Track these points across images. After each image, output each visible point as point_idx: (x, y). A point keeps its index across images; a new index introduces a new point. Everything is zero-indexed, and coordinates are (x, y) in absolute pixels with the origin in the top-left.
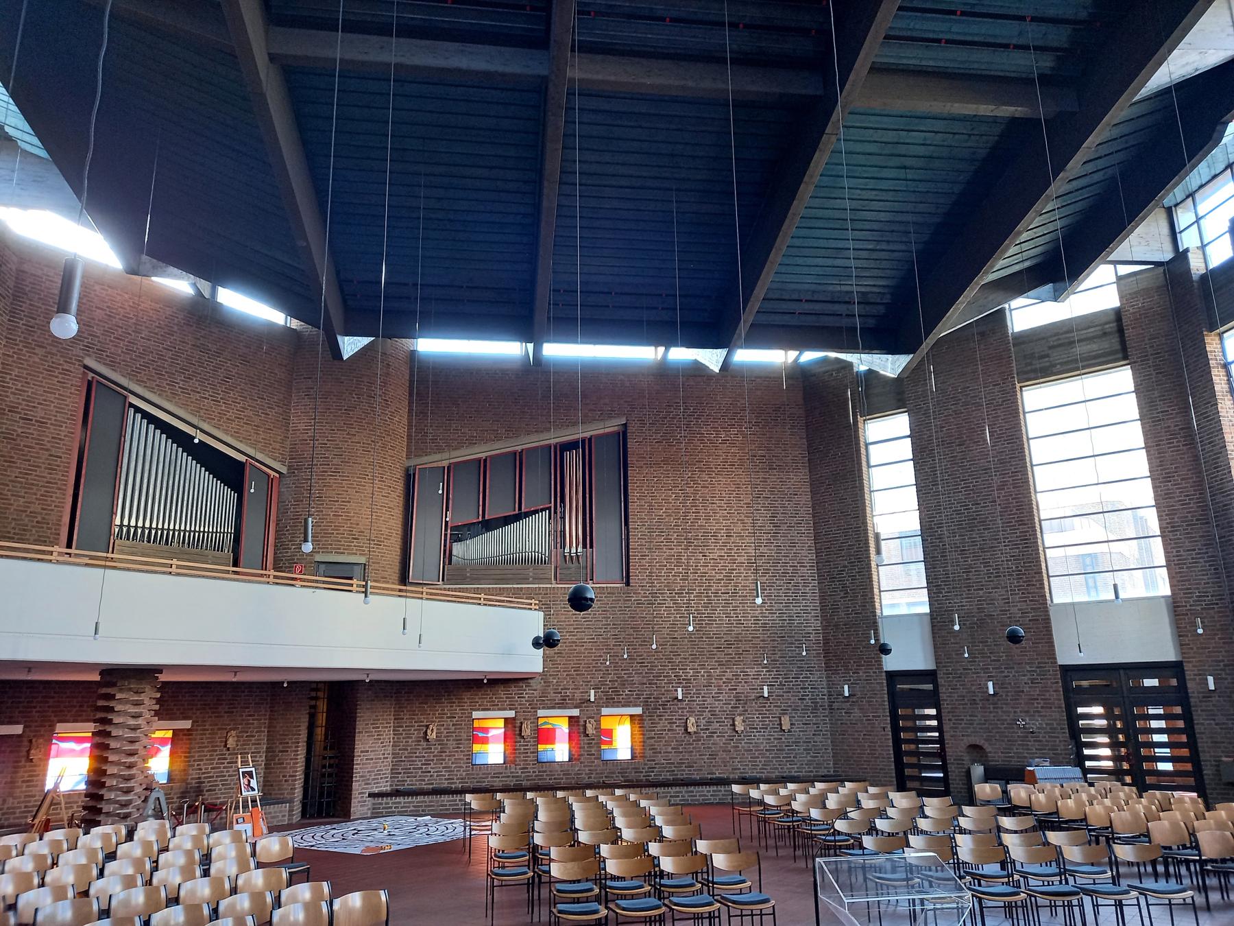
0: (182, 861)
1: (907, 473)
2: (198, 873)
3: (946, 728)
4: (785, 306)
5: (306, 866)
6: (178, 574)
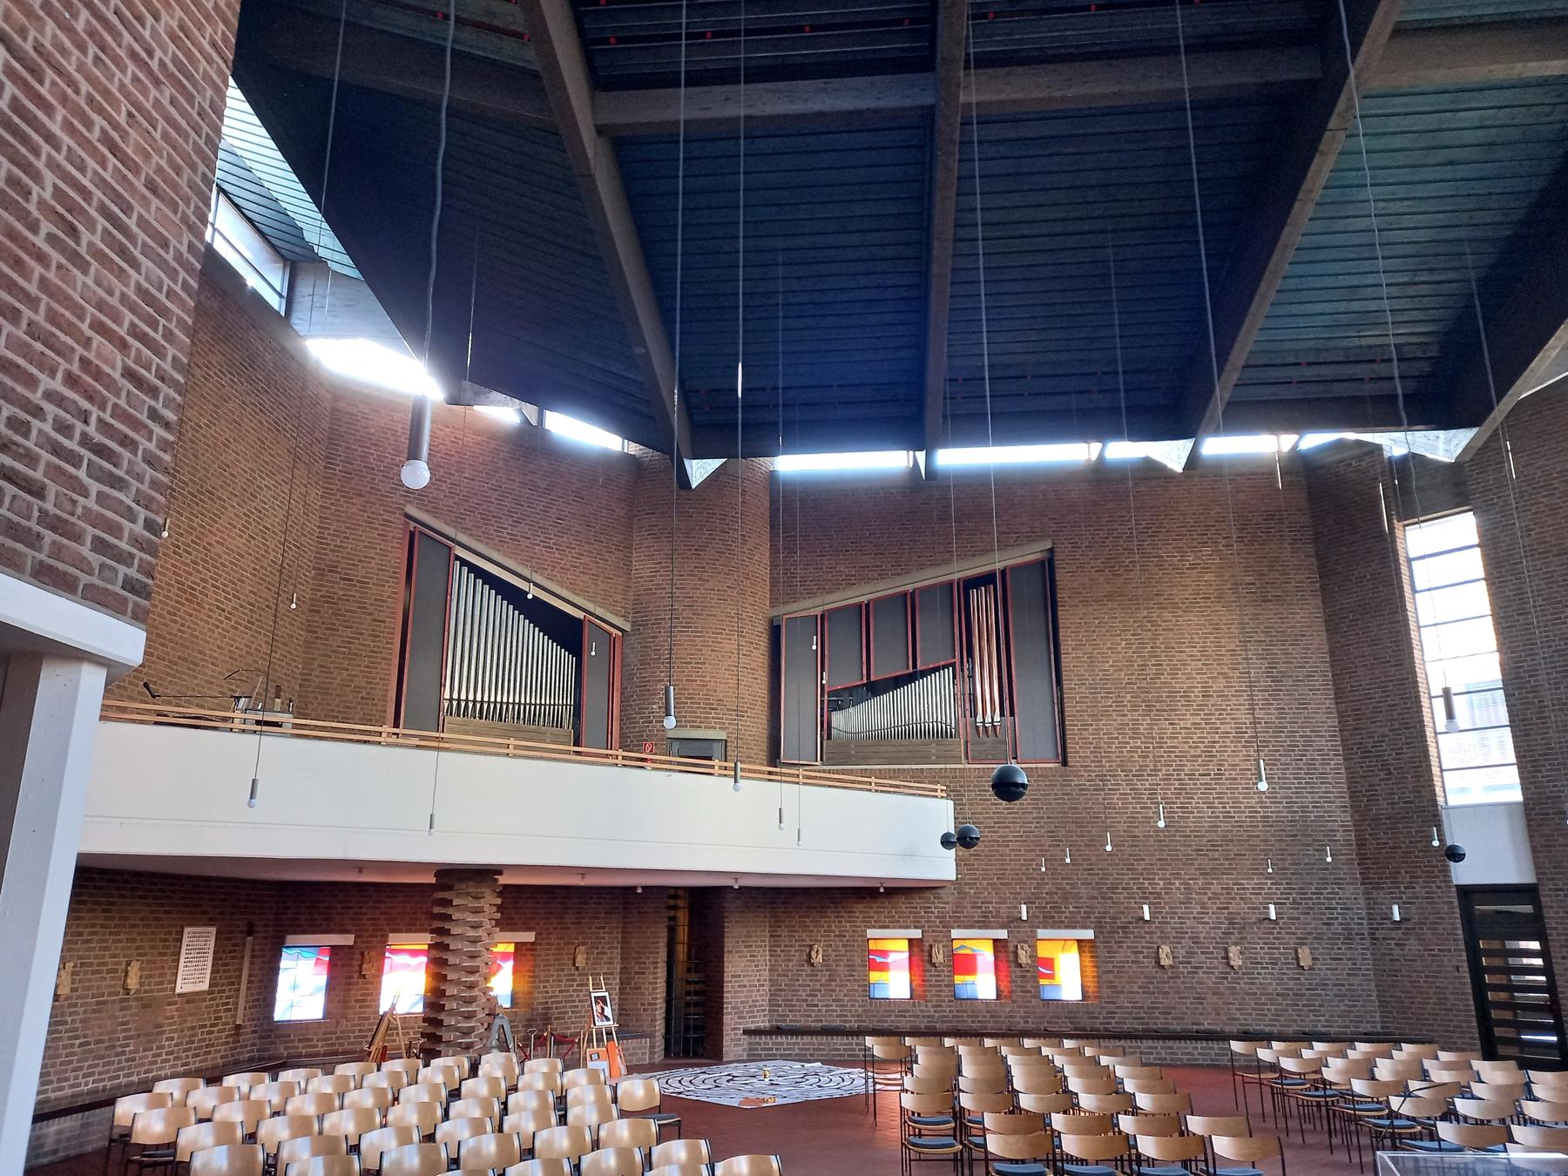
0: (534, 1103)
1: (1478, 599)
2: (554, 1120)
3: (1557, 969)
4: (1274, 374)
5: (679, 1118)
6: (515, 756)
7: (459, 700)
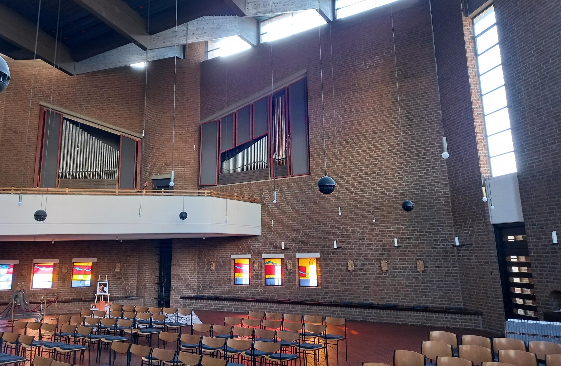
7: (93, 171)
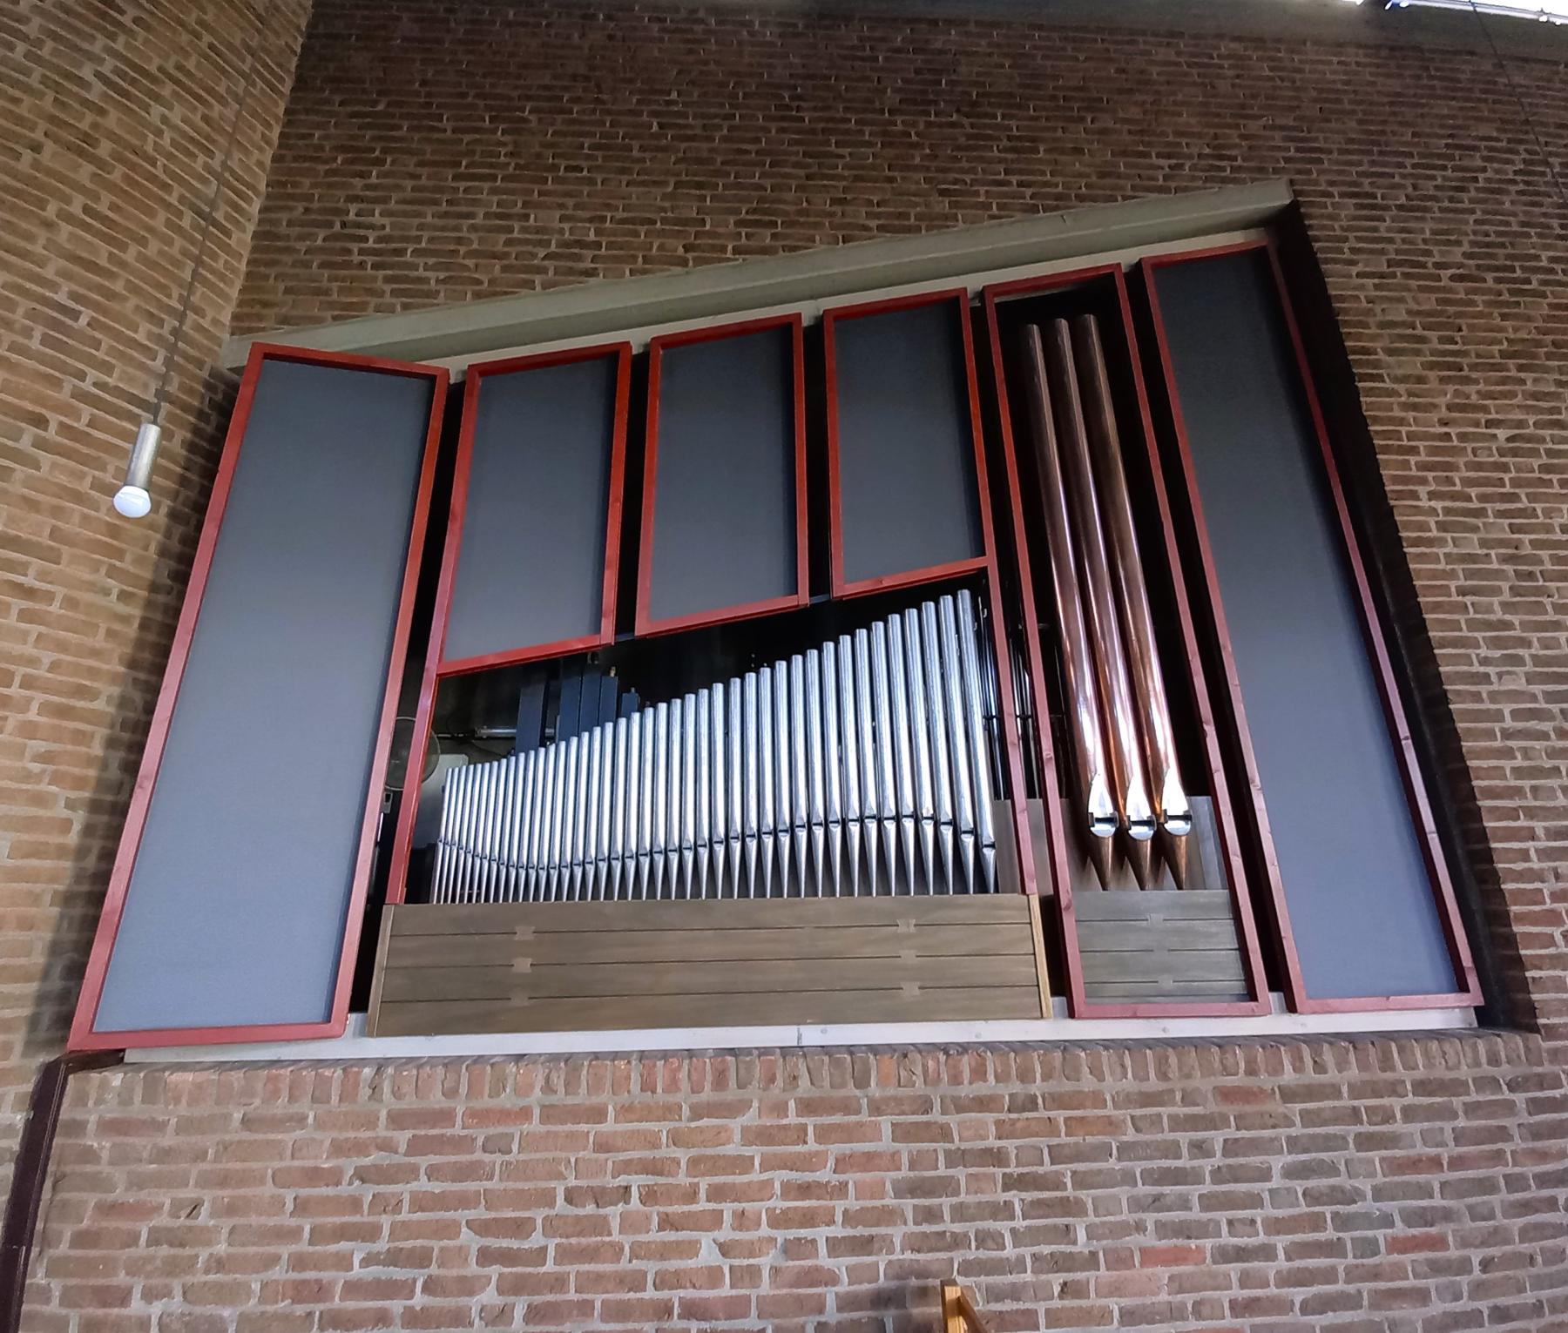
6: (995, 722)
